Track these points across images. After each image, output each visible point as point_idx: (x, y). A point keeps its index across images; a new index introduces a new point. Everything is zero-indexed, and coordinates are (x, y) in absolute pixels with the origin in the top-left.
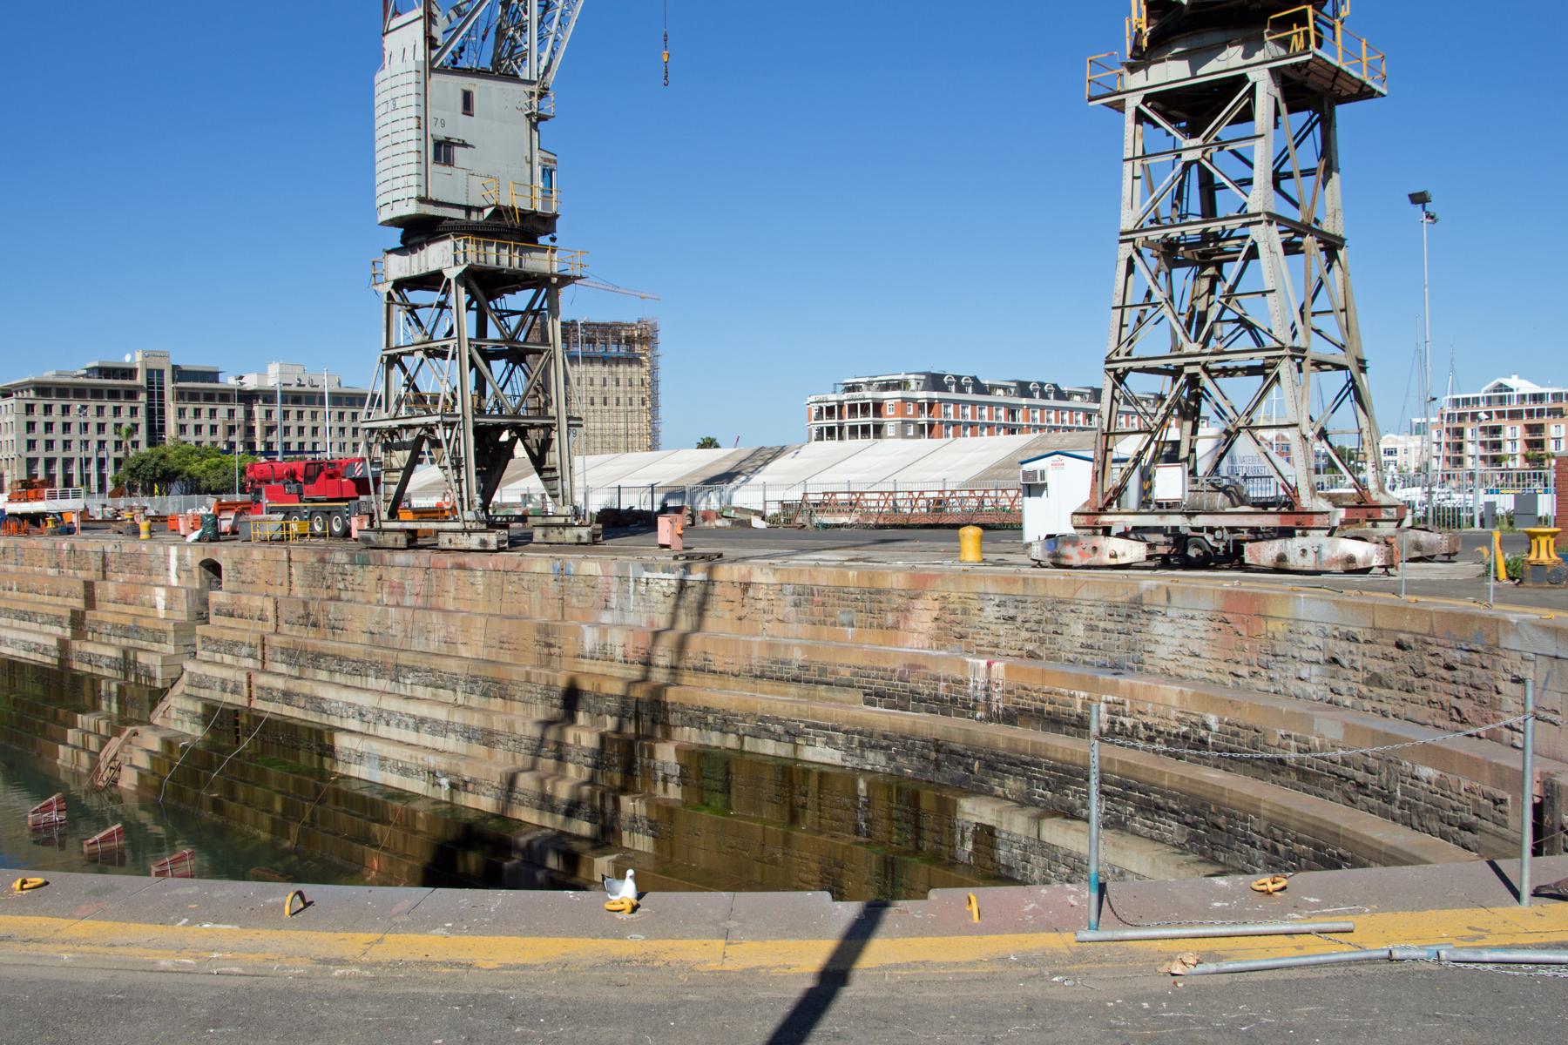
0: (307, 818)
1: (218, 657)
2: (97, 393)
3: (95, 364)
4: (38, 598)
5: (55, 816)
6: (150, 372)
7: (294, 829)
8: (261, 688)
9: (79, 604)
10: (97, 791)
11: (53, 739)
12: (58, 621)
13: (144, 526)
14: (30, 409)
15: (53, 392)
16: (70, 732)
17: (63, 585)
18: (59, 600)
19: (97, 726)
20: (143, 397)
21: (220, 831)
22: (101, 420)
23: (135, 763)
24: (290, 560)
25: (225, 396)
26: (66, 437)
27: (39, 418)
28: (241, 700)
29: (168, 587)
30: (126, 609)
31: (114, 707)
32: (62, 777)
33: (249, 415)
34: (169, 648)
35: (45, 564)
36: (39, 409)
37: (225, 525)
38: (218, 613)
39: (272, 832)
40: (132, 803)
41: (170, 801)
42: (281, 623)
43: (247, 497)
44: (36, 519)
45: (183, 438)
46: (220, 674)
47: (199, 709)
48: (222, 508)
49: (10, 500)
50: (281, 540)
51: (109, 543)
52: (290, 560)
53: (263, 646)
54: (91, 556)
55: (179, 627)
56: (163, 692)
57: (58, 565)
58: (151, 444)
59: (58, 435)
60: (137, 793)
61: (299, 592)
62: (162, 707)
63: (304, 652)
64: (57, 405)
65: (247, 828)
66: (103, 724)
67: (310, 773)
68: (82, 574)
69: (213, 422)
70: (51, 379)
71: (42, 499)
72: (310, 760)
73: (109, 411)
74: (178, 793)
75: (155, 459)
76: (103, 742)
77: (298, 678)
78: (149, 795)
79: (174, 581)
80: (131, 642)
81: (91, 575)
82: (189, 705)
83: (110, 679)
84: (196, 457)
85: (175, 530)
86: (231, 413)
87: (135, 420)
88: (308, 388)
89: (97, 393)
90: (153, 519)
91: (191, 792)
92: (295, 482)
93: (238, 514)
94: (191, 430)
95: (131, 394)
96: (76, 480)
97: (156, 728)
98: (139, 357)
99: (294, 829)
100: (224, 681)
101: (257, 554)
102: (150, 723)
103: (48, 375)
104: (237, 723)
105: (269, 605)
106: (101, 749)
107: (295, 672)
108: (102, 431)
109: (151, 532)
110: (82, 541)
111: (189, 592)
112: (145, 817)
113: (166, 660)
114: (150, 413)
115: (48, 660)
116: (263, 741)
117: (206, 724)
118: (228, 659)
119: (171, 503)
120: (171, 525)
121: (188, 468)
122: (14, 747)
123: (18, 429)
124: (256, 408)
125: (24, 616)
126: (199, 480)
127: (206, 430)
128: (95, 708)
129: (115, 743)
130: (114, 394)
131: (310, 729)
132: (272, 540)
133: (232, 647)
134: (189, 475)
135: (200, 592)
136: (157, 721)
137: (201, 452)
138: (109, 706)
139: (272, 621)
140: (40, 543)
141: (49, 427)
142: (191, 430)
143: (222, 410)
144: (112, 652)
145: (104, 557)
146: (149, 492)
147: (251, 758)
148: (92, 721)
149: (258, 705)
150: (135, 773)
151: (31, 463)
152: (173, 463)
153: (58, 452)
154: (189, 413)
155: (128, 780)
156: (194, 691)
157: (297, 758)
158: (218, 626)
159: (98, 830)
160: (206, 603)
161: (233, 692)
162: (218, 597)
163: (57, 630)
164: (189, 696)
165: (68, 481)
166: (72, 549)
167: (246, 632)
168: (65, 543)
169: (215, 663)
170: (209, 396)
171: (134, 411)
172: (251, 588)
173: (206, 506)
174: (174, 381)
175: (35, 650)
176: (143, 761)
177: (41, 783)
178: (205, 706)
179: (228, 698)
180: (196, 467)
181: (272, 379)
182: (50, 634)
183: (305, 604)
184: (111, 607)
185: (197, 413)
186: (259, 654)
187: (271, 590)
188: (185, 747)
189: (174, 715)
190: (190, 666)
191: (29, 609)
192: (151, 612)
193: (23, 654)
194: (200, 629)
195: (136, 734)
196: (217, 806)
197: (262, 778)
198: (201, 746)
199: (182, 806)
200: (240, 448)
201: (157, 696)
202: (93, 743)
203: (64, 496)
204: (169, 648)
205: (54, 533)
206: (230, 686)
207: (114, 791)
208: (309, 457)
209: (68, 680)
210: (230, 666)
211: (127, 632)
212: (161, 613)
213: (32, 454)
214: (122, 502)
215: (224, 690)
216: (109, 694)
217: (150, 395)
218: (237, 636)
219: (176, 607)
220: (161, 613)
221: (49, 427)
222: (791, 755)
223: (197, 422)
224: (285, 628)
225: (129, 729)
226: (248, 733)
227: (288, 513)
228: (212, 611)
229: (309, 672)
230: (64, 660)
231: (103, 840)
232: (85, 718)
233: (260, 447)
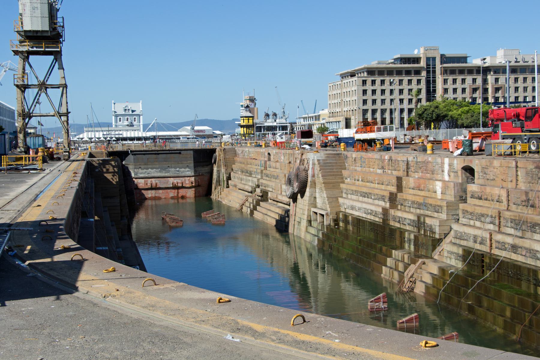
0: (527, 323)
1: (472, 222)
2: (399, 72)
3: (399, 56)
4: (372, 185)
5: (382, 305)
6: (428, 59)
7: (519, 328)
8: (498, 242)
9: (394, 189)
10: (403, 293)
11: (379, 263)
12: (383, 198)
13: (429, 146)
14: (364, 82)
15: (376, 73)
16: (388, 259)
17: (385, 179)
18: (383, 187)
19: (403, 257)
20: (424, 73)
21: (473, 324)
22: (401, 87)
23: (423, 280)
24: (517, 167)
25: (470, 71)
26: (383, 97)
27: (369, 87)
28: (485, 248)
29: (443, 181)
30: (420, 193)
31: (412, 247)
32: (384, 285)
33: (485, 81)
34: (444, 216)
35: (376, 167)
36: (369, 82)
37: (475, 146)
38: (472, 197)
39: (504, 328)
40: (421, 302)
41: (443, 303)
42: (511, 204)
43: (490, 130)
44: (370, 143)
45: (446, 96)
46: (473, 232)
47: (460, 252)
48: (474, 136)
49: (357, 132)
50: (511, 155)
51: (410, 156)
52: (517, 167)
53: (500, 217)
54: (401, 163)
55: (449, 205)
56: (440, 241)
57: (383, 168)
58: (428, 100)
59: (378, 97)
60: (425, 297)
61: (522, 186)
62: (439, 249)
63: (525, 222)
64: (378, 80)
65: (488, 324)
66: (406, 256)
67: (529, 295)
68: (395, 173)
69: (463, 86)
70: (375, 66)
71: (374, 131)
72: (529, 288)
73: (405, 82)
74: (448, 299)
75: (432, 109)
76: (406, 266)
77: (521, 238)
78: (432, 299)
79: (447, 178)
80: (422, 212)
81: (400, 174)
82: (455, 249)
83: (410, 232)
84: (455, 107)
85: (447, 149)
86: (474, 80)
87: (420, 87)
88: (521, 63)
89: (399, 72)
90: (433, 142)
91: (455, 299)
92: (519, 120)
93: (484, 140)
94: (450, 91)
95: (418, 72)
96: (388, 121)
97: (435, 261)
98: (422, 50)
99: (519, 328)
100: (475, 237)
101: (496, 163)
102: (432, 258)
103: (373, 64)
104: (483, 261)
105: (504, 194)
106: (405, 270)
107: (519, 234)
108: (404, 94)
109: (433, 150)
110: (394, 154)
111: (455, 184)
112: (428, 311)
113: (442, 223)
114: (428, 82)
115: (377, 219)
116: (499, 273)
117: (464, 260)
118: (478, 224)
119: (441, 133)
120: (444, 146)
121: (450, 113)
122: (359, 265)
123: (358, 94)
124: (489, 77)
125: (365, 195)
126: (457, 120)
127: (459, 91)
128: (402, 247)
129: (413, 268)
130: (408, 72)
131: (529, 270)
132: (506, 155)
133: (480, 217)
134: (451, 117)
135: (461, 184)
136: (436, 257)
137: (454, 102)
138: (409, 247)
139: (505, 203)
140: (373, 155)
141: (374, 92)
142: (450, 91)
143: (469, 79)
144: (412, 217)
145: (408, 164)
146: (428, 126)
147: (491, 283)
148: (400, 254)
149: (496, 252)
150: (423, 285)
151: (365, 112)
152: (442, 110)
153: (387, 106)
154: (450, 81)
155: (420, 289)
156: (458, 241)
157: (520, 286)
158: (472, 204)
159: (405, 316)
160: (465, 191)
161: (481, 243)
162: (472, 188)
163: (382, 203)
164: (455, 244)
165: (383, 122)
166: (390, 159)
167: (490, 208)
168: (386, 156)
169: (470, 226)
170: (462, 71)
171: (419, 82)
172: (492, 183)
173: (464, 135)
174: (442, 63)
175: (371, 214)
176: (428, 279)
177: (373, 286)
178: (464, 250)
179: (478, 247)
180: (455, 113)
181: (499, 58)
182: (378, 205)
183: (527, 193)
184: (411, 191)
185: (454, 81)
186: (497, 222)
187: (505, 184)
188: (452, 273)
189: (446, 254)
190: (455, 227)
191: (367, 191)
192: (433, 195)
193: (364, 215)
194: (462, 206)
195: (424, 263)
196: (471, 309)
197: (498, 296)
198: (461, 273)
199: (450, 307)
200: (479, 101)
201: (436, 243)
202: (401, 267)
203: (385, 130)
204: (444, 216)
205: (380, 150)
206: (479, 240)
207: (412, 294)
208: (530, 105)
209: (387, 231)
210: (479, 228)
211: (420, 206)
212: (439, 196)
213: (365, 107)
214: (415, 133)
215: (475, 242)
216: (410, 240)
217: (428, 72)
218: (484, 211)
219: (447, 192)
220: (439, 196)
221: (374, 92)
222: (489, 251)
223: (454, 86)
224: (513, 207)
225: (420, 260)
226: (490, 267)
227: (514, 139)
228: (469, 196)
229: (528, 234)
230: (385, 220)
231: (407, 321)
232: (397, 252)
233: (491, 100)
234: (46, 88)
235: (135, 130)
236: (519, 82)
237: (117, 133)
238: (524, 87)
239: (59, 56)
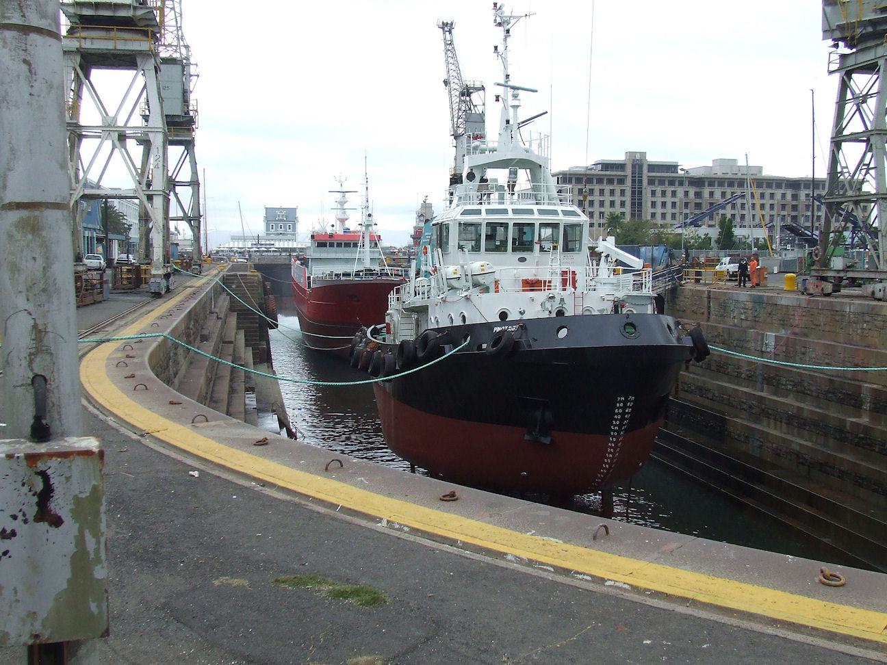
2: (600, 181)
6: (634, 166)
95: (621, 181)
143: (680, 191)
234: (175, 185)
235: (289, 240)
236: (595, 194)
237: (268, 243)
238: (761, 204)
239: (191, 147)
